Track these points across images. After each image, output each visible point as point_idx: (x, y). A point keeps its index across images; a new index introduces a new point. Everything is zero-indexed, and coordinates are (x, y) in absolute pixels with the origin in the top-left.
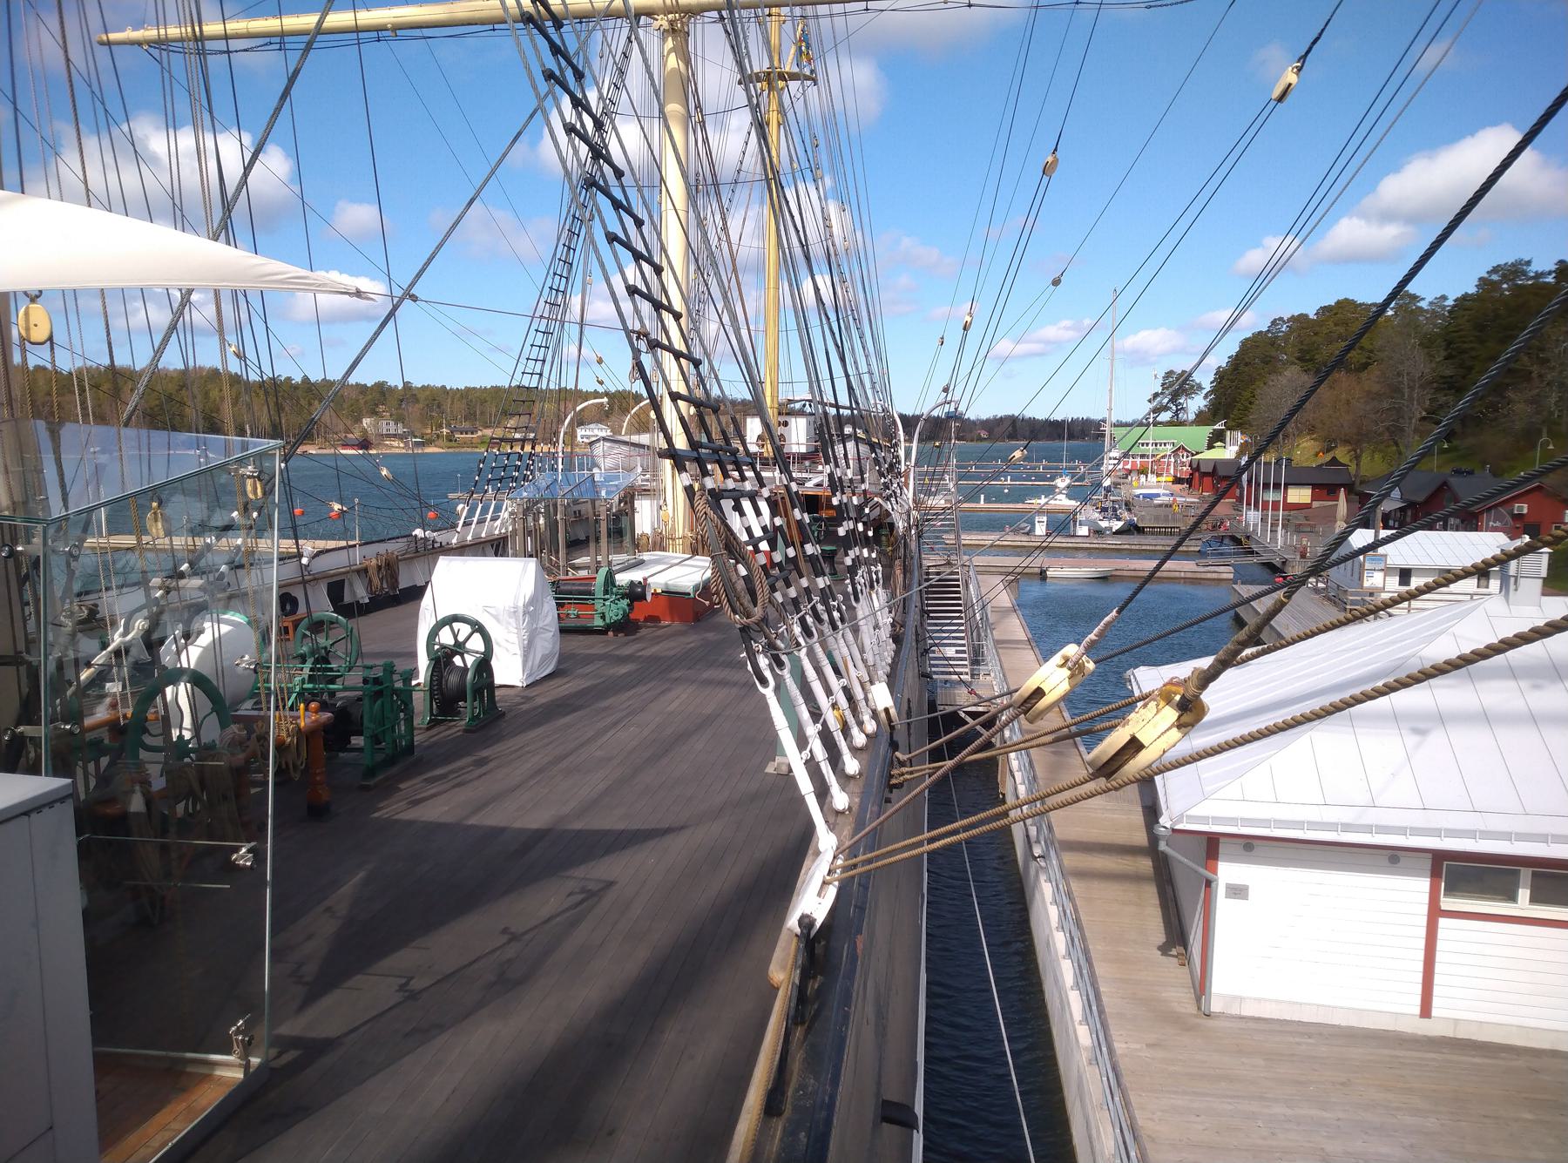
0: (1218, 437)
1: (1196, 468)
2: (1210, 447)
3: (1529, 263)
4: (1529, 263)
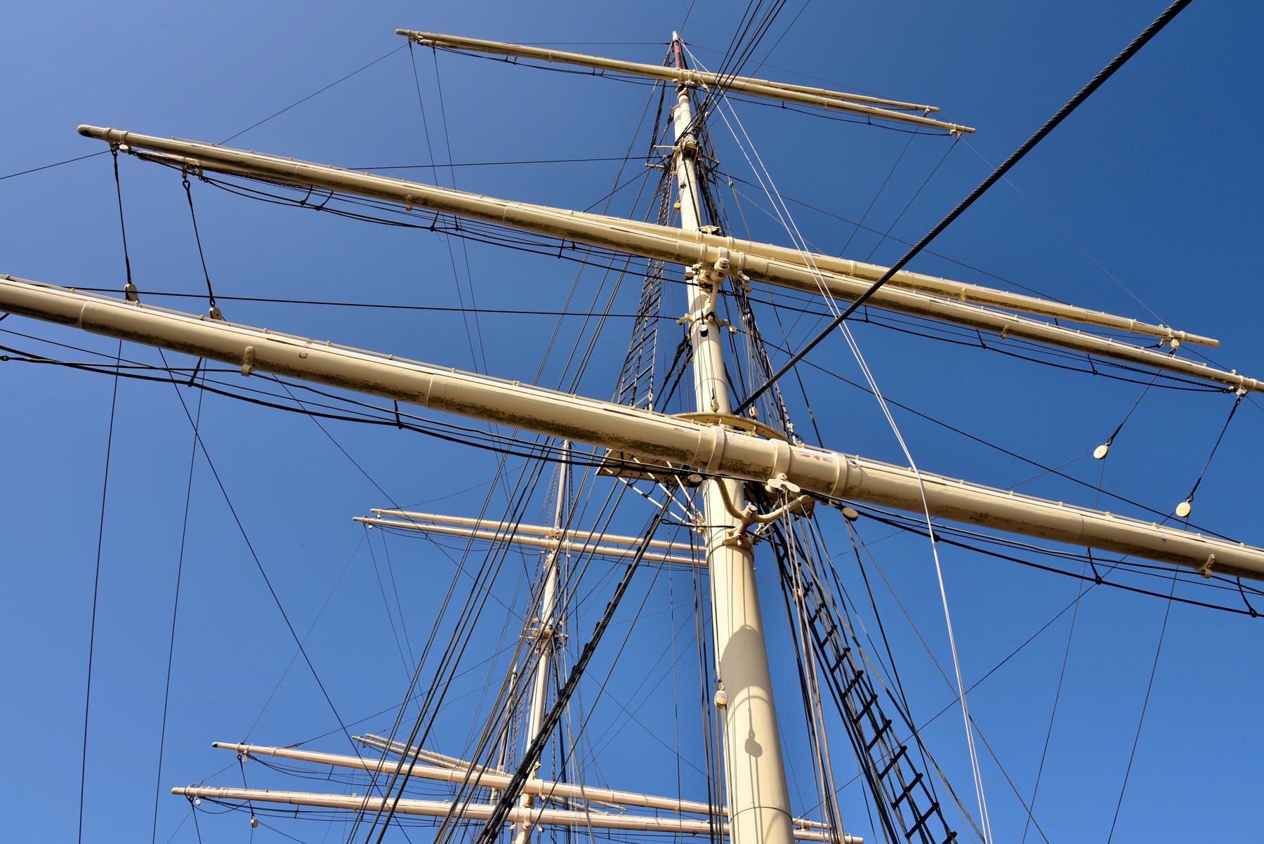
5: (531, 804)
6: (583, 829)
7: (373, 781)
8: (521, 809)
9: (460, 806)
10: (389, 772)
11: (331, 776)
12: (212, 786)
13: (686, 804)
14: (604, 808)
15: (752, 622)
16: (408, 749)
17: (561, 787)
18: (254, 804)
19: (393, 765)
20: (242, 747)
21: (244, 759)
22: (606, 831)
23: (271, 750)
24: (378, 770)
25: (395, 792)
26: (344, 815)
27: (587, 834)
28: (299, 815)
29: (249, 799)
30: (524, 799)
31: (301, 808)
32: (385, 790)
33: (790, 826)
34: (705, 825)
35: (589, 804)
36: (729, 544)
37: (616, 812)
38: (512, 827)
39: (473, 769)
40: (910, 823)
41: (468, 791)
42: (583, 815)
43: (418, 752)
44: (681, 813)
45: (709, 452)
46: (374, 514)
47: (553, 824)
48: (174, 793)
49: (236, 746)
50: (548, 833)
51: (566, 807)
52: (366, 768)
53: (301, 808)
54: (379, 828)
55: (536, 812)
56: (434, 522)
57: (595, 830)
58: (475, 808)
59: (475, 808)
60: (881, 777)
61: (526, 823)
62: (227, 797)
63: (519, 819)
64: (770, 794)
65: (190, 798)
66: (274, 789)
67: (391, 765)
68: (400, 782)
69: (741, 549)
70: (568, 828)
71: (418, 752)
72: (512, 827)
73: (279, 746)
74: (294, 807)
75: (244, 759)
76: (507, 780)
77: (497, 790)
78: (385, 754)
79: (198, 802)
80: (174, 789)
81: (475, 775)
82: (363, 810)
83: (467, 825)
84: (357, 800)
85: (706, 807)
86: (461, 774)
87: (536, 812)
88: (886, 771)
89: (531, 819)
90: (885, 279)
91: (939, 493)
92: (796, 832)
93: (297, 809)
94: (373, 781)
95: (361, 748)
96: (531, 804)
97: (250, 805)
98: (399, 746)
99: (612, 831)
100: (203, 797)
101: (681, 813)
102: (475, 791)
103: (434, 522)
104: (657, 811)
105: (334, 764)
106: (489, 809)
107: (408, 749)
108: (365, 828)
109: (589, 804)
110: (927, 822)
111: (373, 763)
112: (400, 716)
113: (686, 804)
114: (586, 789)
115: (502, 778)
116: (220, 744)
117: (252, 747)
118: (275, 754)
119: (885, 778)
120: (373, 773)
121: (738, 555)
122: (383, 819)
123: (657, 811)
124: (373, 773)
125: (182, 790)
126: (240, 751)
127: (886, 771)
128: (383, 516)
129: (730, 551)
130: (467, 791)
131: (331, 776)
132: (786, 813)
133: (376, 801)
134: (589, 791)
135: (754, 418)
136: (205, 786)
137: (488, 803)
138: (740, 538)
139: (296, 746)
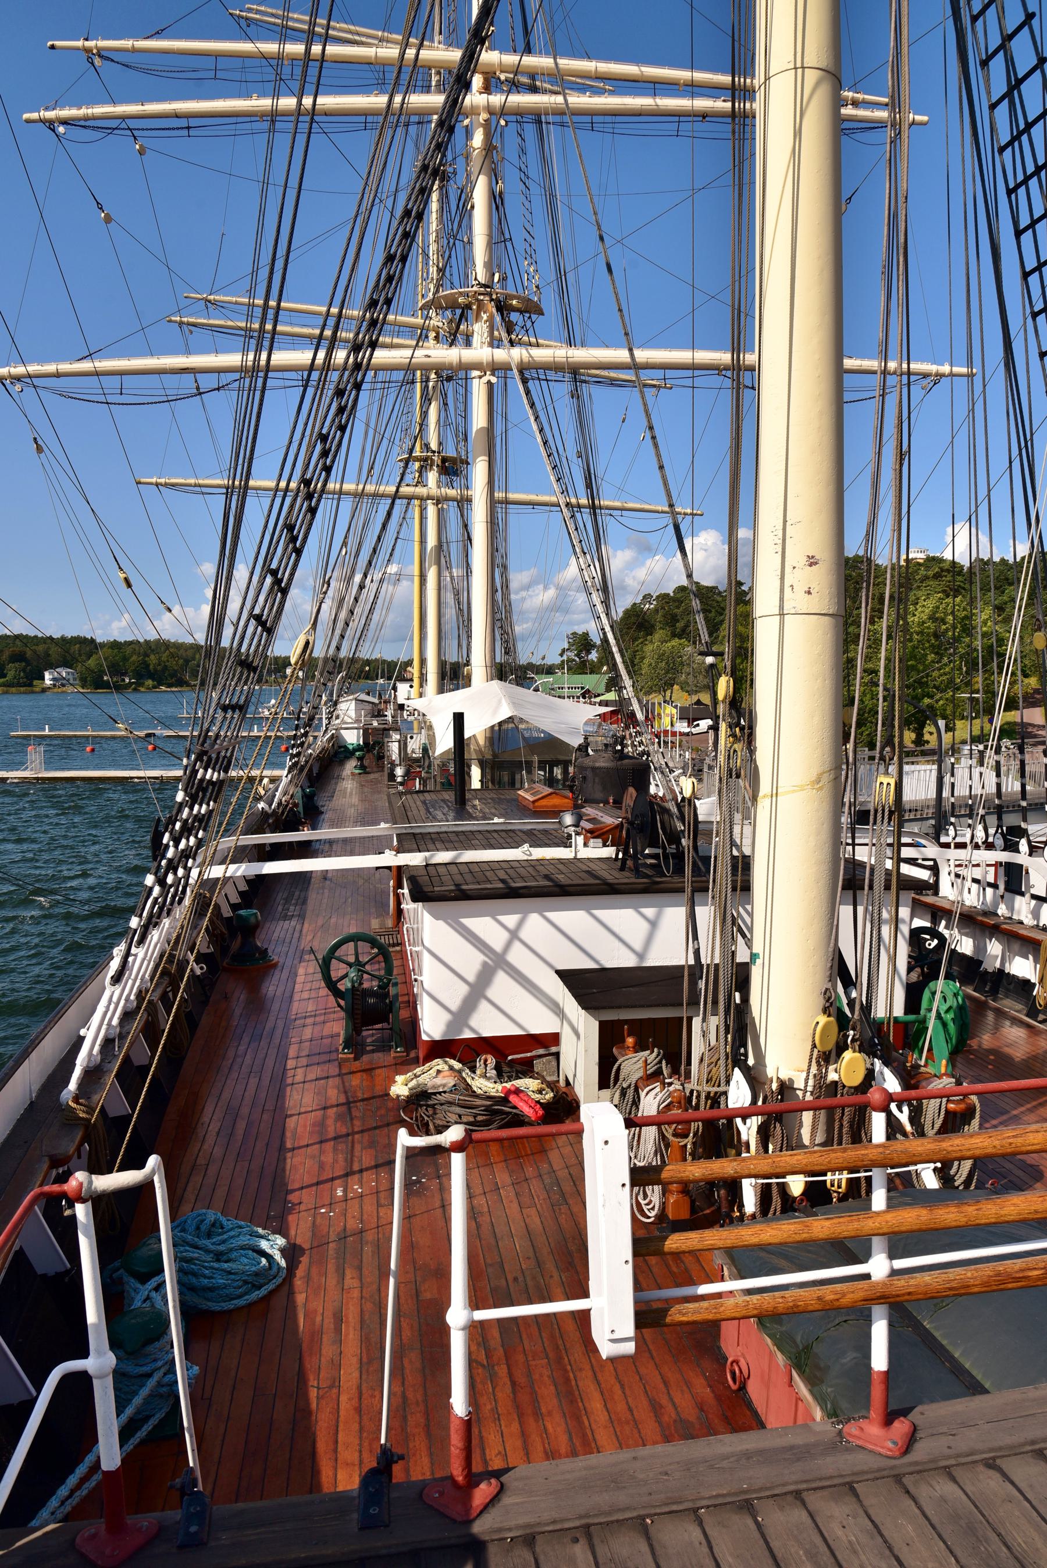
5: (487, 89)
6: (558, 119)
7: (276, 74)
8: (475, 98)
9: (398, 99)
10: (293, 59)
11: (214, 73)
12: (71, 106)
13: (700, 76)
14: (582, 89)
16: (313, 24)
17: (529, 61)
18: (132, 124)
19: (299, 48)
20: (88, 44)
21: (97, 61)
22: (588, 119)
23: (128, 43)
24: (279, 57)
25: (310, 87)
26: (248, 126)
27: (562, 125)
28: (192, 132)
29: (124, 118)
30: (477, 81)
31: (193, 122)
32: (296, 86)
33: (838, 102)
34: (723, 105)
35: (561, 81)
37: (600, 92)
38: (466, 122)
39: (406, 45)
40: (1000, 87)
41: (405, 77)
42: (560, 99)
43: (328, 27)
44: (693, 89)
47: (520, 114)
48: (28, 121)
49: (79, 43)
50: (513, 126)
51: (534, 90)
52: (263, 56)
53: (193, 122)
54: (301, 139)
55: (496, 99)
57: (575, 119)
58: (417, 100)
59: (417, 100)
60: (974, 19)
61: (484, 116)
62: (94, 118)
63: (474, 111)
64: (816, 53)
65: (50, 124)
66: (152, 100)
67: (296, 48)
68: (313, 71)
70: (537, 117)
71: (328, 27)
72: (466, 122)
73: (136, 37)
74: (184, 123)
75: (97, 61)
76: (456, 55)
77: (439, 73)
78: (284, 34)
79: (61, 129)
80: (26, 116)
81: (410, 53)
82: (273, 116)
83: (407, 125)
84: (266, 103)
85: (727, 79)
86: (391, 52)
87: (496, 99)
88: (982, 12)
89: (489, 109)
92: (844, 111)
93: (188, 123)
94: (276, 74)
95: (246, 29)
96: (487, 89)
98: (299, 19)
99: (596, 119)
100: (65, 122)
101: (693, 89)
102: (407, 76)
104: (656, 87)
106: (437, 100)
107: (313, 24)
108: (283, 141)
109: (561, 81)
110: (1022, 87)
111: (270, 47)
112: (1025, 331)
113: (700, 76)
115: (444, 54)
116: (58, 43)
118: (134, 50)
119: (980, 23)
120: (274, 62)
122: (303, 127)
123: (656, 87)
124: (274, 62)
125: (35, 116)
126: (88, 50)
127: (982, 12)
130: (407, 76)
131: (214, 73)
132: (835, 77)
133: (288, 103)
134: (566, 63)
136: (62, 108)
137: (428, 92)
139: (158, 34)
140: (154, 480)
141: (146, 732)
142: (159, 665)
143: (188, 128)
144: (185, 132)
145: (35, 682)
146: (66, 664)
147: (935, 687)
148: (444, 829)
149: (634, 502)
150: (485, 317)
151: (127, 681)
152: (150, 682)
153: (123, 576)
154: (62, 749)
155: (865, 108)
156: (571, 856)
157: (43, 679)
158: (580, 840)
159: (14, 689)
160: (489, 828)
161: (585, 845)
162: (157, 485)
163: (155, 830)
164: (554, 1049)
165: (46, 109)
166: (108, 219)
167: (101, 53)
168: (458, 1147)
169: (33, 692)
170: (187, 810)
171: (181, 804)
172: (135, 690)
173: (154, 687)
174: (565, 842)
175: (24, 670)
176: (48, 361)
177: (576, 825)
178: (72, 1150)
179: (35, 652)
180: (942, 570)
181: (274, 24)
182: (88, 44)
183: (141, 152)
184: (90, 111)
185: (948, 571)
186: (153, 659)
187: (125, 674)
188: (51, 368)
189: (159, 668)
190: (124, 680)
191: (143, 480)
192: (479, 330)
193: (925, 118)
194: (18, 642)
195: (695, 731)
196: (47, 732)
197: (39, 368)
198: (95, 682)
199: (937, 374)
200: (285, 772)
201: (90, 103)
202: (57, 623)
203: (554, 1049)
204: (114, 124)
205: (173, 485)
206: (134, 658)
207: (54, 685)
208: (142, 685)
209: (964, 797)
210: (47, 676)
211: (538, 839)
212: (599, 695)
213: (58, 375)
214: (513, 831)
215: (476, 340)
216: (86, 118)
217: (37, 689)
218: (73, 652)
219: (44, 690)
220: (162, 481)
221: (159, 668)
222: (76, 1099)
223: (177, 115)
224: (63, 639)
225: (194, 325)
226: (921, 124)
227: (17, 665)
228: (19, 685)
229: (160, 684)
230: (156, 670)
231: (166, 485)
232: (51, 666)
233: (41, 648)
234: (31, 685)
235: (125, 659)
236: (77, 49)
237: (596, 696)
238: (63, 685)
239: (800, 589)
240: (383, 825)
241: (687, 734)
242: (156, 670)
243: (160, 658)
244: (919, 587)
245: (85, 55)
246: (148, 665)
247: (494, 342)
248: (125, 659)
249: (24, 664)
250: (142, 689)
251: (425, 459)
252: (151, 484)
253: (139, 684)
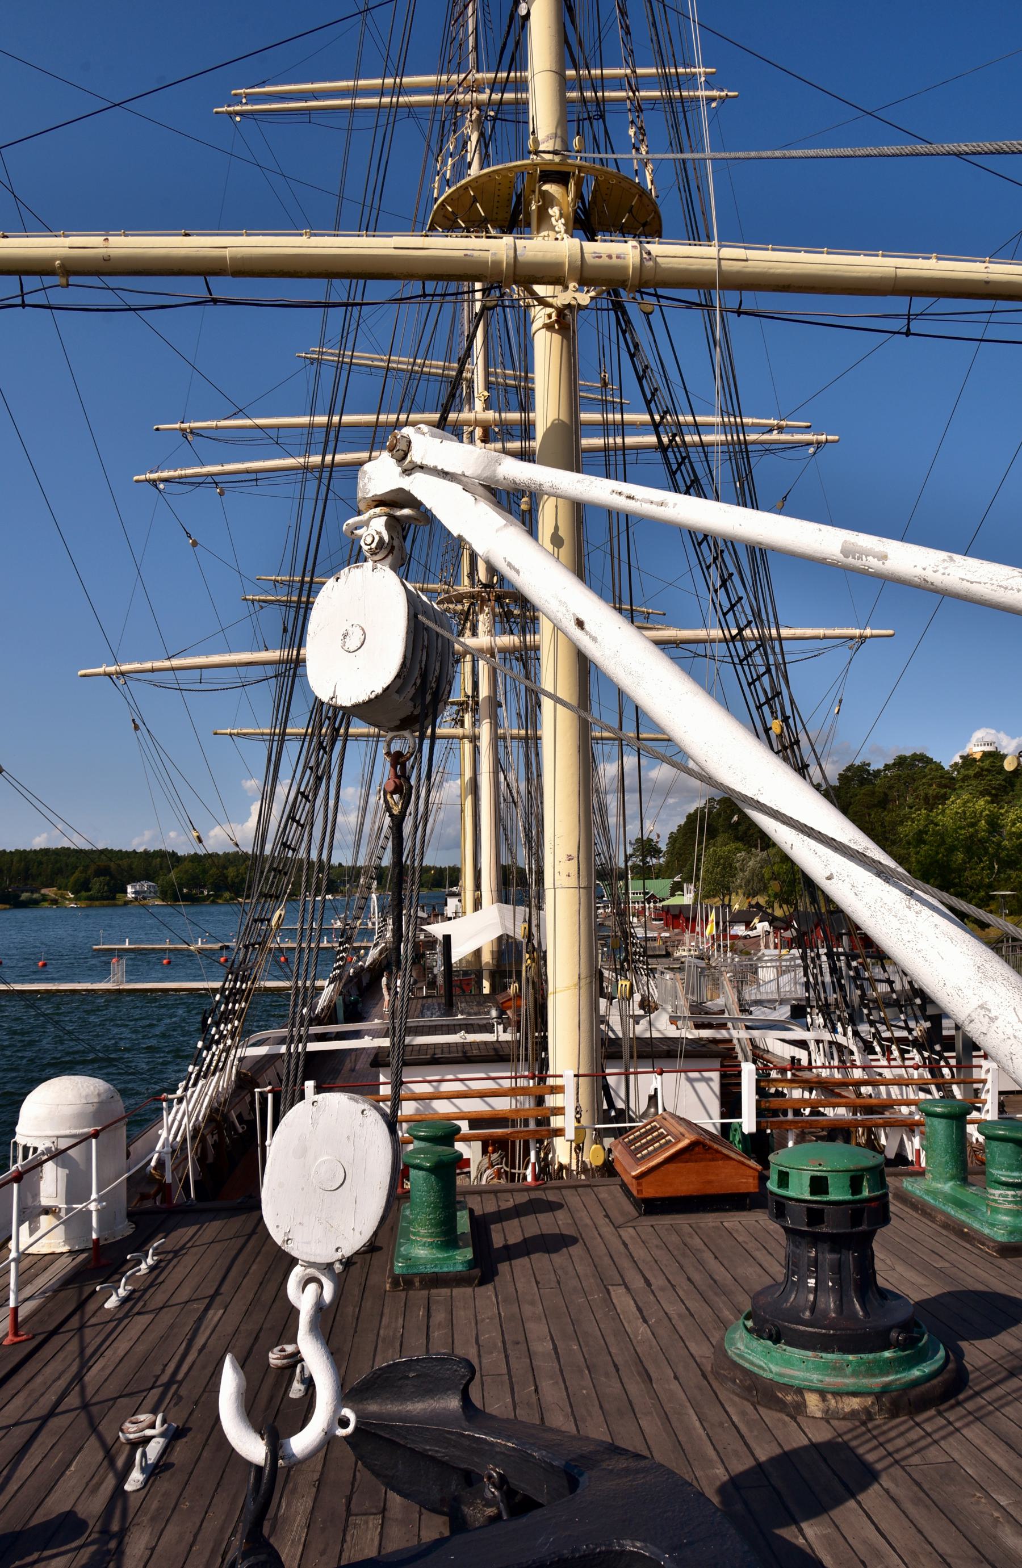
0: (677, 888)
1: (667, 909)
2: (673, 895)
3: (869, 765)
4: (869, 765)
12: (169, 469)
15: (564, 417)
18: (217, 479)
20: (185, 425)
23: (213, 424)
36: (548, 327)
45: (501, 273)
46: (237, 99)
48: (137, 481)
49: (177, 426)
56: (315, 95)
62: (186, 477)
65: (154, 483)
69: (558, 332)
74: (253, 476)
79: (161, 486)
80: (135, 478)
90: (85, 1365)
91: (738, 273)
97: (212, 480)
103: (315, 95)
105: (279, 427)
114: (503, 415)
116: (161, 427)
117: (193, 425)
118: (217, 428)
121: (557, 338)
125: (142, 477)
126: (183, 430)
128: (252, 99)
129: (549, 334)
135: (578, 152)
138: (556, 321)
140: (228, 731)
141: (221, 944)
142: (237, 877)
143: (257, 480)
144: (254, 483)
145: (118, 896)
146: (148, 878)
147: (967, 886)
148: (421, 1024)
149: (648, 733)
150: (486, 610)
151: (206, 893)
152: (227, 895)
153: (195, 834)
154: (140, 961)
155: (787, 433)
156: (495, 1039)
157: (126, 892)
158: (501, 1028)
159: (97, 903)
160: (455, 1022)
161: (505, 1031)
162: (231, 735)
163: (203, 1014)
164: (466, 1170)
165: (151, 472)
166: (195, 544)
167: (192, 431)
168: (270, 1091)
169: (116, 905)
170: (223, 1006)
171: (218, 1002)
172: (213, 902)
173: (232, 899)
174: (488, 1029)
175: (108, 884)
176: (146, 661)
177: (499, 1017)
178: (152, 1192)
179: (119, 865)
180: (982, 770)
181: (333, 361)
182: (185, 425)
183: (221, 494)
184: (183, 472)
185: (988, 770)
186: (231, 872)
187: (204, 887)
188: (148, 665)
189: (237, 880)
190: (202, 892)
191: (219, 731)
192: (483, 620)
193: (837, 438)
194: (103, 857)
195: (752, 933)
196: (127, 946)
197: (139, 666)
198: (171, 895)
199: (861, 637)
200: (327, 982)
201: (183, 467)
202: (140, 840)
203: (466, 1170)
204: (201, 479)
205: (245, 734)
206: (214, 870)
207: (136, 899)
208: (219, 897)
209: (887, 993)
210: (130, 889)
211: (470, 1028)
212: (664, 900)
213: (153, 670)
214: (472, 1025)
215: (482, 628)
216: (180, 477)
217: (120, 903)
218: (152, 865)
219: (126, 903)
220: (235, 731)
221: (237, 880)
222: (155, 1168)
223: (248, 472)
224: (146, 852)
225: (265, 601)
226: (833, 442)
227: (102, 878)
228: (103, 898)
229: (238, 894)
230: (234, 883)
231: (238, 735)
232: (133, 880)
233: (125, 863)
234: (114, 898)
235: (205, 872)
236: (176, 429)
237: (661, 901)
238: (145, 898)
239: (564, 874)
240: (376, 1021)
241: (745, 937)
242: (234, 883)
243: (238, 870)
244: (961, 787)
245: (181, 433)
246: (226, 878)
247: (490, 633)
248: (205, 872)
249: (108, 878)
250: (220, 901)
251: (461, 704)
252: (226, 734)
253: (217, 896)
